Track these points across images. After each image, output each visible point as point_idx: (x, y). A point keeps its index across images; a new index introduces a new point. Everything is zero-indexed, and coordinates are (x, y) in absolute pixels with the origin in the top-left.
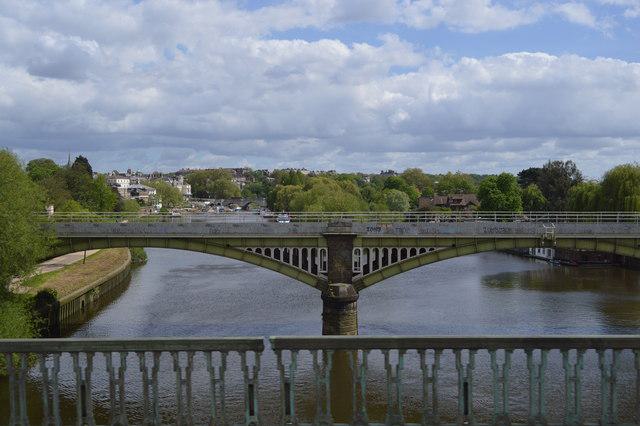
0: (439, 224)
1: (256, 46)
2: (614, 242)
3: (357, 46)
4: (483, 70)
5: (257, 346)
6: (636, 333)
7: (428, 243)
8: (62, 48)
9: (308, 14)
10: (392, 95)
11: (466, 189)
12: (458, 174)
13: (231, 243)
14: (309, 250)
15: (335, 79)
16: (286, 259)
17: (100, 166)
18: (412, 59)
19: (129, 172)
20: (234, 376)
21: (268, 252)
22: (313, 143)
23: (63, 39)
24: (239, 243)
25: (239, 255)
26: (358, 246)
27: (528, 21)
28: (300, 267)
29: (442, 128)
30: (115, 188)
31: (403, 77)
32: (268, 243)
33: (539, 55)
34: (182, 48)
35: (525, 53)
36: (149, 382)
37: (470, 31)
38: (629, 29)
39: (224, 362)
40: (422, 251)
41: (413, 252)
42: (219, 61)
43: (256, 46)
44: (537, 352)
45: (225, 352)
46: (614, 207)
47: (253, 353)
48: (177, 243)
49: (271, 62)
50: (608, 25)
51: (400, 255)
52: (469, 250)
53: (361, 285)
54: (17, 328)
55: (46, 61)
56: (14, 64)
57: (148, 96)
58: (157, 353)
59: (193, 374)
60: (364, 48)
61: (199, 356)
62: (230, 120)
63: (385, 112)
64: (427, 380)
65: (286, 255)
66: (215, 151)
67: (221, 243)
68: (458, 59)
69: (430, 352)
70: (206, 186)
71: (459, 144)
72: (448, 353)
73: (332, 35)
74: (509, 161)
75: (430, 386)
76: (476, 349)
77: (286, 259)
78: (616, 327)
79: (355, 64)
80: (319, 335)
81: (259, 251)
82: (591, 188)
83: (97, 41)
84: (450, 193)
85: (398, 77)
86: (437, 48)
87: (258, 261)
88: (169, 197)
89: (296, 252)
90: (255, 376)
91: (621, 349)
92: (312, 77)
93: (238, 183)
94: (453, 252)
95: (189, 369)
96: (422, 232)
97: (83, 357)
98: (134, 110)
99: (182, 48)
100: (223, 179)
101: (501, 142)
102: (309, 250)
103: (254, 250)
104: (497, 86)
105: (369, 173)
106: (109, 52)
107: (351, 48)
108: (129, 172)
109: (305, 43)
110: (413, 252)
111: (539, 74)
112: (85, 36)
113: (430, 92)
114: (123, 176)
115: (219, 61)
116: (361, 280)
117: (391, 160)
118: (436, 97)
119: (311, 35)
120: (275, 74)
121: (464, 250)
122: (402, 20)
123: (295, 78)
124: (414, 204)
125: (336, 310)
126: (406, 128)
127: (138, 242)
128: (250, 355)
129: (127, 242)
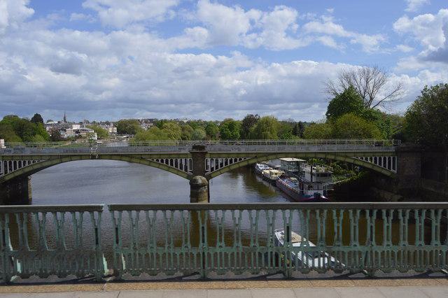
1: (169, 57)
2: (335, 154)
3: (220, 57)
4: (282, 69)
5: (99, 209)
6: (266, 201)
7: (243, 156)
8: (68, 57)
9: (194, 41)
10: (237, 82)
13: (348, 155)
15: (209, 74)
16: (172, 164)
18: (247, 63)
20: (88, 226)
21: (162, 161)
22: (198, 106)
23: (69, 53)
24: (353, 155)
26: (208, 156)
27: (304, 45)
28: (382, 166)
29: (264, 97)
31: (243, 73)
32: (162, 156)
33: (310, 62)
34: (131, 58)
35: (303, 61)
36: (79, 227)
37: (276, 50)
38: (353, 50)
40: (240, 159)
41: (236, 160)
42: (150, 64)
43: (169, 57)
47: (135, 211)
48: (115, 157)
49: (176, 65)
50: (342, 47)
53: (209, 178)
55: (59, 64)
56: (44, 66)
57: (114, 82)
58: (28, 213)
59: (258, 221)
60: (223, 58)
62: (157, 94)
63: (234, 91)
64: (252, 225)
66: (149, 111)
67: (343, 154)
68: (270, 64)
70: (124, 128)
71: (271, 106)
72: (86, 213)
73: (207, 52)
75: (271, 222)
77: (172, 164)
78: (264, 198)
79: (219, 66)
80: (189, 203)
81: (157, 160)
83: (87, 55)
85: (241, 73)
86: (260, 58)
87: (157, 165)
88: (101, 134)
92: (197, 72)
95: (274, 218)
96: (32, 152)
98: (107, 89)
99: (131, 58)
100: (134, 125)
101: (292, 105)
103: (155, 160)
104: (290, 77)
106: (93, 60)
107: (217, 58)
109: (194, 55)
110: (236, 160)
111: (310, 71)
112: (80, 52)
113: (257, 80)
115: (150, 64)
117: (238, 114)
118: (259, 83)
119: (196, 51)
120: (178, 71)
122: (242, 44)
123: (189, 73)
125: (196, 190)
126: (244, 98)
128: (96, 213)
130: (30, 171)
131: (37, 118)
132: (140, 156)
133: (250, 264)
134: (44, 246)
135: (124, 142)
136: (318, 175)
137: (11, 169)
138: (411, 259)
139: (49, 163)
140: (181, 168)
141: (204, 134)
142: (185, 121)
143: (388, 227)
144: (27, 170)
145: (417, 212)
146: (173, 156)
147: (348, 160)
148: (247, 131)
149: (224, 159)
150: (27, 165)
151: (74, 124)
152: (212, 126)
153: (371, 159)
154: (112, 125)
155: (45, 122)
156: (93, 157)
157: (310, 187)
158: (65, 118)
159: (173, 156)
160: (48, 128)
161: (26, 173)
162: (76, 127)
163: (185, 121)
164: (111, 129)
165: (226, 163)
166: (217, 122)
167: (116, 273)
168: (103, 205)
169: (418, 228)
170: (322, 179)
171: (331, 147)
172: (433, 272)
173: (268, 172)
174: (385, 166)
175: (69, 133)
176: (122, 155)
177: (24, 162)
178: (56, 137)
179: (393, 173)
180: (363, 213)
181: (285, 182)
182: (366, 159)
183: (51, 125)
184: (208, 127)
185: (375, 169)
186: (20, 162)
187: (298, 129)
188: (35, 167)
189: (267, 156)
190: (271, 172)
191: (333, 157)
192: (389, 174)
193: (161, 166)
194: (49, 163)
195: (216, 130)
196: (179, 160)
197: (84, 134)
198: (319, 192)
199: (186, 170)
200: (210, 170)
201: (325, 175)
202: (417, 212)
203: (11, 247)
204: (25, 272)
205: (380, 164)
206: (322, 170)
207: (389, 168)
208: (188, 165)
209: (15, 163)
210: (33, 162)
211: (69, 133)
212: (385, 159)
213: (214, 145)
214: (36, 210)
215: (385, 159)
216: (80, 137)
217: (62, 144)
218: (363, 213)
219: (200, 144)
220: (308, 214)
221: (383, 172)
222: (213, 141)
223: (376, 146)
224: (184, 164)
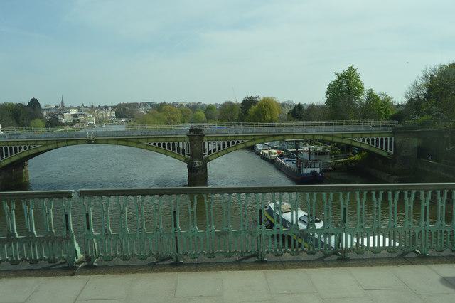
2: (332, 135)
5: (68, 195)
13: (140, 140)
16: (169, 148)
21: (159, 145)
24: (350, 136)
40: (238, 142)
41: (233, 143)
44: (140, 197)
48: (112, 141)
67: (135, 140)
70: (123, 111)
77: (169, 148)
81: (154, 144)
87: (155, 149)
102: (13, 147)
110: (233, 143)
121: (131, 144)
130: (28, 156)
131: (34, 103)
133: (289, 247)
134: (14, 233)
135: (121, 127)
136: (316, 154)
137: (7, 155)
140: (179, 151)
141: (203, 116)
142: (184, 105)
143: (442, 207)
144: (23, 155)
145: (422, 193)
146: (374, 135)
147: (345, 141)
148: (246, 114)
149: (221, 142)
150: (23, 150)
151: (72, 108)
152: (212, 109)
153: (368, 141)
154: (110, 109)
155: (42, 106)
156: (89, 142)
157: (308, 165)
158: (62, 102)
160: (45, 113)
161: (23, 158)
162: (74, 112)
163: (184, 105)
164: (109, 113)
165: (224, 146)
166: (217, 105)
167: (88, 259)
168: (73, 191)
169: (423, 209)
170: (320, 158)
171: (328, 128)
172: (407, 253)
173: (266, 152)
174: (382, 147)
175: (66, 118)
176: (119, 140)
177: (20, 148)
178: (53, 122)
179: (389, 154)
180: (369, 195)
181: (282, 161)
182: (364, 140)
183: (48, 110)
184: (209, 110)
185: (372, 149)
186: (16, 148)
187: (298, 112)
188: (31, 152)
189: (264, 138)
190: (269, 152)
191: (330, 139)
192: (385, 154)
194: (45, 148)
195: (217, 113)
196: (176, 143)
197: (81, 118)
198: (316, 169)
199: (184, 153)
200: (207, 153)
201: (321, 154)
202: (422, 193)
205: (377, 145)
206: (319, 149)
207: (386, 149)
208: (185, 148)
209: (11, 148)
210: (29, 147)
211: (66, 118)
212: (382, 139)
213: (207, 128)
214: (34, 196)
215: (382, 139)
216: (78, 121)
217: (59, 130)
218: (369, 195)
219: (198, 127)
220: (365, 196)
221: (381, 153)
222: (212, 124)
223: (373, 127)
224: (181, 147)
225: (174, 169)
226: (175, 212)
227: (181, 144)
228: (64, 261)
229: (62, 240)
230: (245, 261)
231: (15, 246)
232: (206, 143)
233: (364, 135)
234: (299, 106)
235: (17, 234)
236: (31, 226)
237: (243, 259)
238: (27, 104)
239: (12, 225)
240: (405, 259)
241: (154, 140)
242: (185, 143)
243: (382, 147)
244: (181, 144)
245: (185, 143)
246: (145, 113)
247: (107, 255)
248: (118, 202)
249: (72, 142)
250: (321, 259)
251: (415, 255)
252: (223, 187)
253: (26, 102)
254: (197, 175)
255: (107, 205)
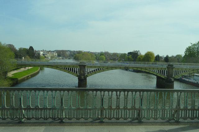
0: (110, 63)
2: (141, 68)
7: (72, 67)
11: (117, 56)
12: (15, 48)
14: (180, 71)
17: (36, 48)
19: (43, 50)
21: (66, 69)
24: (149, 69)
25: (60, 69)
26: (86, 67)
30: (39, 54)
39: (128, 94)
40: (187, 71)
41: (185, 71)
45: (128, 92)
46: (156, 59)
51: (99, 69)
52: (110, 69)
54: (6, 84)
61: (130, 93)
65: (70, 69)
67: (56, 66)
69: (46, 92)
70: (61, 54)
74: (125, 50)
76: (64, 91)
81: (64, 68)
82: (141, 56)
84: (114, 57)
87: (64, 70)
89: (73, 69)
90: (142, 97)
91: (73, 91)
93: (68, 53)
94: (107, 69)
97: (142, 92)
100: (39, 52)
102: (180, 71)
105: (97, 52)
108: (43, 50)
110: (185, 71)
114: (42, 51)
116: (87, 75)
124: (106, 58)
127: (42, 67)
129: (39, 66)
132: (145, 68)
134: (5, 106)
138: (128, 125)
139: (20, 67)
140: (75, 72)
159: (159, 69)
174: (162, 74)
192: (163, 77)
193: (66, 71)
199: (77, 73)
203: (23, 106)
204: (29, 117)
205: (160, 73)
208: (77, 71)
221: (162, 76)
224: (76, 70)
225: (72, 80)
226: (20, 98)
227: (76, 69)
228: (18, 119)
229: (17, 109)
230: (133, 122)
231: (4, 111)
232: (87, 69)
233: (66, 67)
234: (167, 56)
235: (23, 106)
236: (4, 103)
237: (132, 121)
238: (28, 48)
239: (4, 102)
240: (170, 122)
241: (64, 66)
242: (78, 69)
243: (162, 74)
244: (76, 69)
245: (78, 69)
246: (131, 56)
247: (62, 117)
248: (125, 94)
249: (119, 68)
250: (130, 122)
251: (174, 121)
252: (103, 88)
253: (28, 48)
254: (82, 81)
255: (38, 95)
